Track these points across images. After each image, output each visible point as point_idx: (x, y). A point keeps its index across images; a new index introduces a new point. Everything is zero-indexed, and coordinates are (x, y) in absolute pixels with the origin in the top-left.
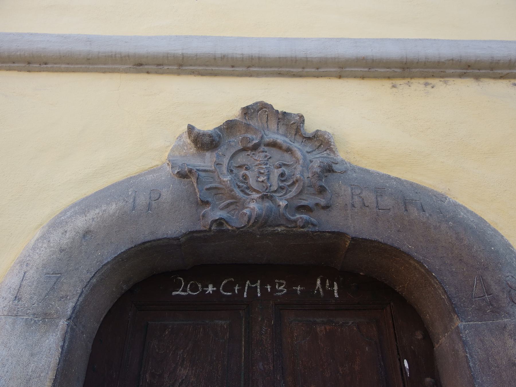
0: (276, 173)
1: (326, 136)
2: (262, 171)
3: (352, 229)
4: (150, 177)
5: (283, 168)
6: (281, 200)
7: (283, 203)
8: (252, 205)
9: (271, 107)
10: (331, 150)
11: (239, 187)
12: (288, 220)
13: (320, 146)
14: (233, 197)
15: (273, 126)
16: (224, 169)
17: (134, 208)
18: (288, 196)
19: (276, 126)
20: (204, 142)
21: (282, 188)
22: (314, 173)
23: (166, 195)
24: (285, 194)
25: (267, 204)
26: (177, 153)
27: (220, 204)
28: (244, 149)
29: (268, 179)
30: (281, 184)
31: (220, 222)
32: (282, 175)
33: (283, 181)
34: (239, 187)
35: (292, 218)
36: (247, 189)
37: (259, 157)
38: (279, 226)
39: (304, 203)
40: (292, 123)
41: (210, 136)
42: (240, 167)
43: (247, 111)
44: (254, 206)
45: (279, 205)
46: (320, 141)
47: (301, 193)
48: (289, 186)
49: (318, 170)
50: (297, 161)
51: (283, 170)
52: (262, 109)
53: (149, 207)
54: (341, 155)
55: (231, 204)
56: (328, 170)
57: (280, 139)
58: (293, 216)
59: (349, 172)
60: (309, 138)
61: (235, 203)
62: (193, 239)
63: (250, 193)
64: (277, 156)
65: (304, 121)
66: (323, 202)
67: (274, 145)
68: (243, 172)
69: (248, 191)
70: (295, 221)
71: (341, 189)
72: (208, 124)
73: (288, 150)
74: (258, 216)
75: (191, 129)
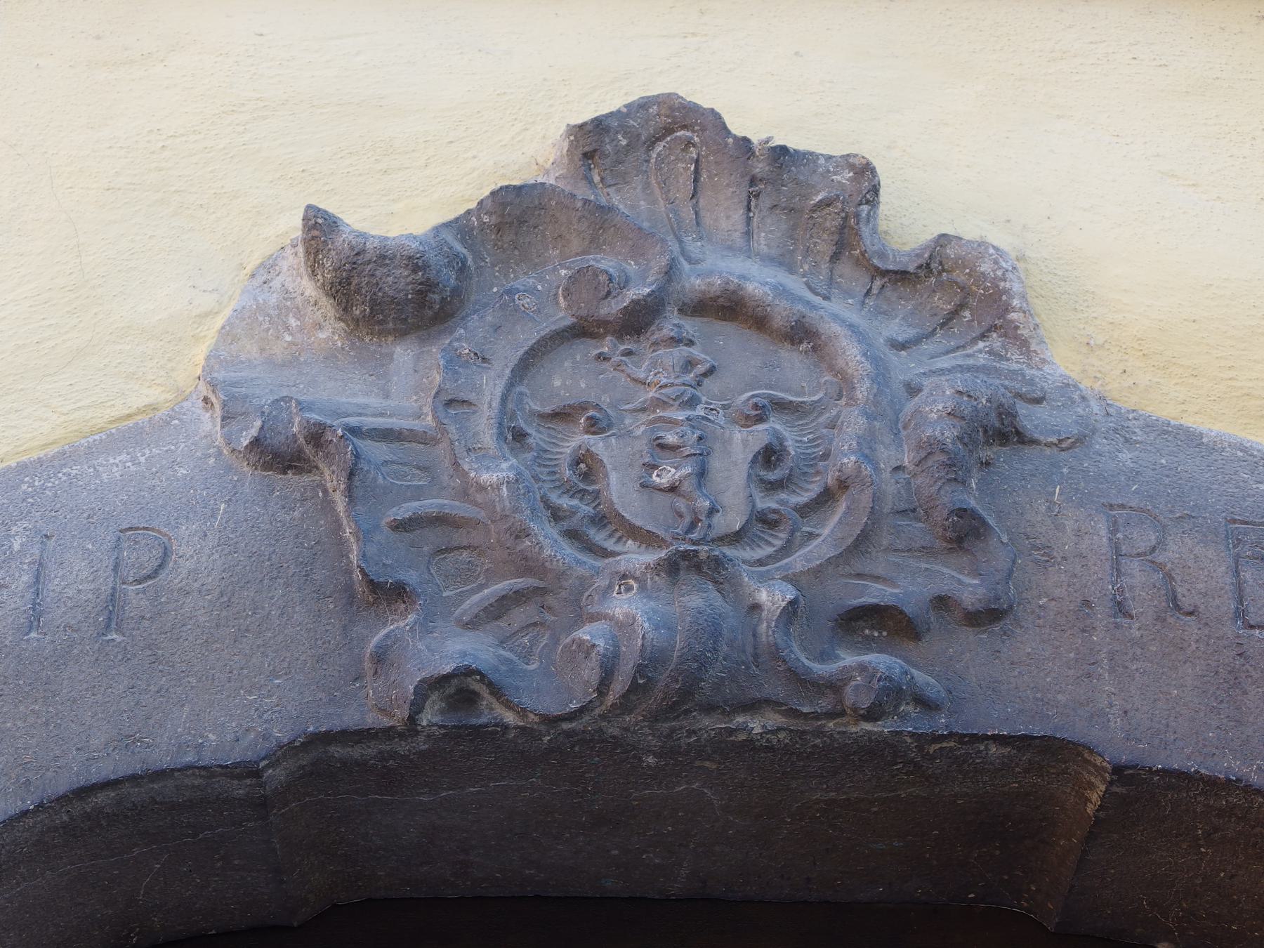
0: (741, 444)
1: (986, 267)
2: (671, 438)
3: (1116, 723)
4: (115, 466)
5: (775, 424)
6: (764, 579)
7: (772, 597)
8: (622, 605)
9: (712, 122)
10: (1010, 332)
11: (556, 515)
12: (800, 680)
13: (955, 313)
14: (529, 565)
15: (725, 213)
16: (484, 427)
17: (35, 616)
18: (798, 561)
19: (738, 215)
20: (389, 295)
21: (768, 521)
22: (930, 448)
23: (196, 554)
24: (785, 551)
25: (697, 599)
26: (249, 349)
27: (462, 597)
28: (582, 330)
29: (702, 474)
30: (766, 503)
31: (460, 688)
32: (770, 455)
33: (773, 487)
34: (556, 515)
35: (822, 669)
36: (595, 527)
37: (656, 366)
38: (752, 706)
39: (876, 594)
40: (818, 202)
41: (415, 263)
42: (563, 415)
43: (594, 143)
44: (631, 611)
45: (756, 607)
46: (958, 290)
47: (861, 543)
48: (804, 510)
49: (949, 433)
50: (845, 386)
51: (776, 434)
52: (669, 130)
53: (112, 611)
54: (1063, 359)
55: (519, 597)
56: (998, 431)
57: (758, 279)
58: (823, 657)
59: (1100, 444)
60: (901, 277)
61: (537, 596)
62: (328, 769)
63: (610, 545)
64: (743, 362)
65: (875, 190)
66: (970, 589)
67: (729, 307)
68: (576, 439)
69: (598, 537)
70: (834, 686)
71: (1060, 528)
72: (404, 209)
73: (801, 334)
74: (651, 661)
75: (319, 227)
